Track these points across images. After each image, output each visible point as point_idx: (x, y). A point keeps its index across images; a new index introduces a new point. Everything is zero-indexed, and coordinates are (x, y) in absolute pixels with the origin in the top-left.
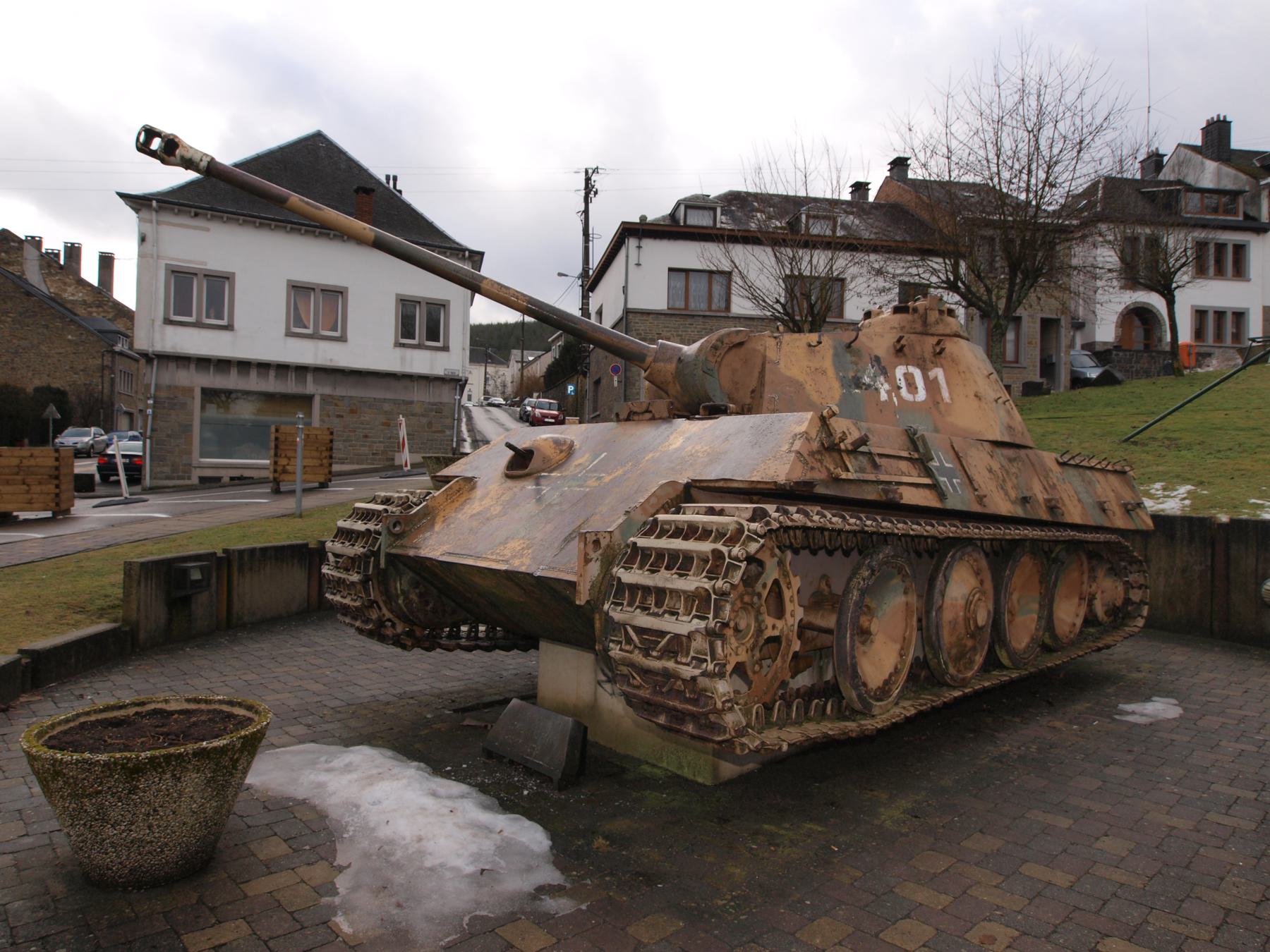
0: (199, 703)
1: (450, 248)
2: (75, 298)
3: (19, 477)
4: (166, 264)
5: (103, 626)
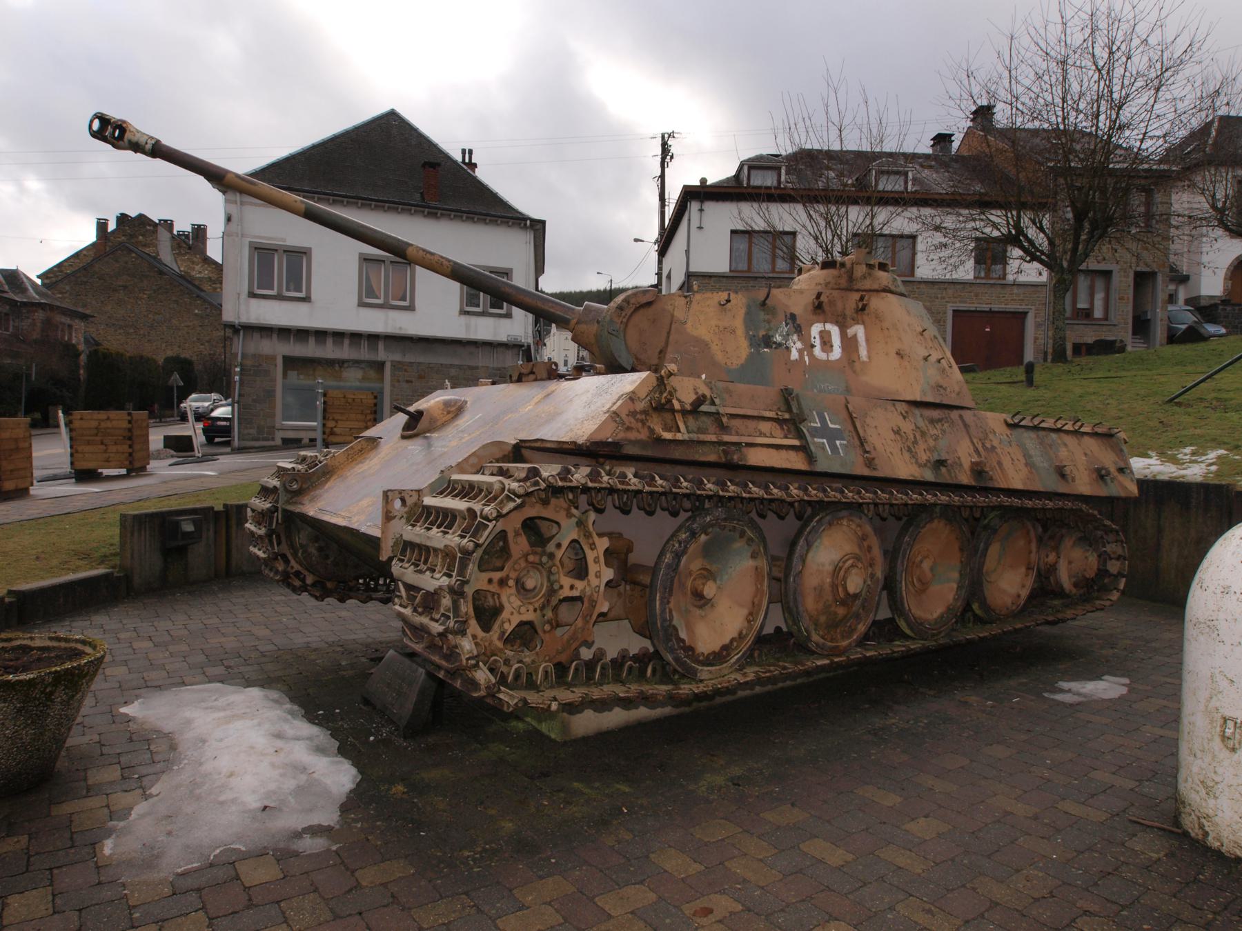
0: (60, 641)
1: (512, 218)
2: (202, 275)
3: (98, 438)
4: (250, 242)
5: (101, 571)
